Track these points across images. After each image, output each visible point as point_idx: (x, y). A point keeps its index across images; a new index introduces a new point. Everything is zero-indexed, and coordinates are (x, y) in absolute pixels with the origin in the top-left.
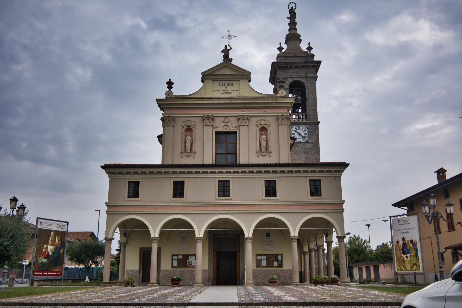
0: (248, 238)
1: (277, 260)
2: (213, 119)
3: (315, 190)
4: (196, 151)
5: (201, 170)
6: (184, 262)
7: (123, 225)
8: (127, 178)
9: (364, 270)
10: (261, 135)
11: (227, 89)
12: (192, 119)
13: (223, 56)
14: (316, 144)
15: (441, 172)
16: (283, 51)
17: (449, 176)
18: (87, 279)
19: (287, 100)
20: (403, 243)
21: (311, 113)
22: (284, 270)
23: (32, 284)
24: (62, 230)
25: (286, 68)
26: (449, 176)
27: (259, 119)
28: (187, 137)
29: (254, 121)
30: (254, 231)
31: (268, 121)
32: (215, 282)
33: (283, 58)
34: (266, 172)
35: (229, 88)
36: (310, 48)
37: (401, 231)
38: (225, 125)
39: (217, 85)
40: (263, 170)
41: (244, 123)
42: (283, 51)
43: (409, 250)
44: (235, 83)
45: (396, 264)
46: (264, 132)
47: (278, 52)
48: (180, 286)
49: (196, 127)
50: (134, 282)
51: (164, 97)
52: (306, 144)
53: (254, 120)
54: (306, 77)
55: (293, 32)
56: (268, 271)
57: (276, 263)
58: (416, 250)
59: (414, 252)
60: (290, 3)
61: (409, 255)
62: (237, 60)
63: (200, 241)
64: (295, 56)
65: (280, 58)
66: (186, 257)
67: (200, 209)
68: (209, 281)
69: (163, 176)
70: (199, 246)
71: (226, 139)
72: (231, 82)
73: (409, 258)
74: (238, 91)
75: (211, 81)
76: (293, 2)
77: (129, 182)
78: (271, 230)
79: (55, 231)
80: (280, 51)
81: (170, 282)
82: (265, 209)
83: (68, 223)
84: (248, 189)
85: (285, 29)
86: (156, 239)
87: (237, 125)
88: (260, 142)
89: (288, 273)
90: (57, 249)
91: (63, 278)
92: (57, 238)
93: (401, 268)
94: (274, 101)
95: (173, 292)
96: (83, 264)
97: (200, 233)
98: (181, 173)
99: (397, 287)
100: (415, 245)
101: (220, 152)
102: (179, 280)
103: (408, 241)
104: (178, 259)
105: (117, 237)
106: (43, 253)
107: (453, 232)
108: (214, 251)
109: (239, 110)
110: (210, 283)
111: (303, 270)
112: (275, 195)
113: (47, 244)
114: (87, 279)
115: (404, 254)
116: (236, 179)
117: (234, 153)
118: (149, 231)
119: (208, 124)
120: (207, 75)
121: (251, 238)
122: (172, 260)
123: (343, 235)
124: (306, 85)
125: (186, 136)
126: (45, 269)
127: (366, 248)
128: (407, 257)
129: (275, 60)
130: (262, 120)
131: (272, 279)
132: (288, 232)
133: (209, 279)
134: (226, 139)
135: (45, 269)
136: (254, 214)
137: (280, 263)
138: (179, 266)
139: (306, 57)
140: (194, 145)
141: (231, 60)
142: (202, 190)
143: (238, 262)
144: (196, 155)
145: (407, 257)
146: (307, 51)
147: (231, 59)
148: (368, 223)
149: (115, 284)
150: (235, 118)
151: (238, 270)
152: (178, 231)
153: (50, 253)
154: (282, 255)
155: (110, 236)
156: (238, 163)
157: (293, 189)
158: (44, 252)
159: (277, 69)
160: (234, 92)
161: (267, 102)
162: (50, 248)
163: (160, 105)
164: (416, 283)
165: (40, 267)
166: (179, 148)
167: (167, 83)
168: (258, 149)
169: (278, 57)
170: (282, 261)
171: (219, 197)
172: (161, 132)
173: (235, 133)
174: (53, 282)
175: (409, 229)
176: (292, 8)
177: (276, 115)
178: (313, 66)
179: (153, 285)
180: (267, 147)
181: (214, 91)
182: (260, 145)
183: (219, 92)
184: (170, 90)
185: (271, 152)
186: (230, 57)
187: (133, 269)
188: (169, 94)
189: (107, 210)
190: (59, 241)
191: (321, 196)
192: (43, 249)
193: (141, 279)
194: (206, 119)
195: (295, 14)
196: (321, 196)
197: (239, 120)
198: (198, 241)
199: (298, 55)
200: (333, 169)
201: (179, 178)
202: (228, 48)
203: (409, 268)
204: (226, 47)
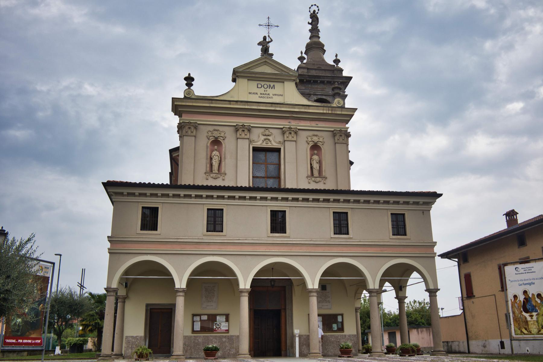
1: (336, 322)
2: (249, 130)
3: (399, 226)
4: (227, 172)
10: (312, 155)
11: (267, 93)
15: (511, 215)
16: (305, 61)
17: (521, 219)
18: (58, 351)
22: (345, 336)
26: (521, 219)
28: (214, 153)
31: (321, 137)
33: (306, 71)
35: (270, 91)
36: (337, 61)
37: (522, 282)
38: (265, 139)
39: (253, 86)
40: (332, 197)
44: (277, 85)
45: (513, 326)
46: (316, 152)
49: (226, 140)
55: (315, 40)
57: (335, 326)
60: (312, 5)
61: (534, 314)
64: (319, 69)
65: (302, 70)
67: (246, 248)
69: (193, 201)
72: (272, 84)
73: (535, 318)
74: (282, 95)
76: (315, 5)
78: (342, 281)
80: (302, 62)
81: (203, 354)
85: (305, 38)
88: (311, 164)
91: (44, 348)
93: (522, 331)
94: (330, 112)
101: (258, 174)
102: (216, 350)
103: (533, 295)
104: (201, 320)
114: (58, 351)
115: (527, 311)
116: (294, 208)
117: (278, 177)
119: (243, 136)
120: (241, 72)
122: (193, 322)
125: (212, 151)
126: (19, 334)
128: (531, 316)
131: (346, 348)
135: (19, 334)
137: (340, 326)
139: (333, 71)
140: (223, 163)
141: (272, 55)
142: (248, 221)
143: (283, 325)
145: (531, 316)
147: (272, 55)
150: (279, 131)
152: (212, 280)
154: (342, 315)
160: (276, 96)
161: (322, 111)
164: (469, 352)
167: (186, 79)
170: (342, 323)
173: (278, 150)
174: (6, 354)
175: (533, 279)
176: (314, 11)
177: (333, 129)
180: (320, 171)
181: (250, 93)
182: (312, 168)
183: (257, 96)
184: (189, 88)
185: (326, 178)
186: (270, 52)
187: (135, 335)
188: (189, 94)
195: (318, 19)
197: (284, 133)
200: (421, 200)
201: (215, 204)
202: (267, 40)
204: (265, 38)
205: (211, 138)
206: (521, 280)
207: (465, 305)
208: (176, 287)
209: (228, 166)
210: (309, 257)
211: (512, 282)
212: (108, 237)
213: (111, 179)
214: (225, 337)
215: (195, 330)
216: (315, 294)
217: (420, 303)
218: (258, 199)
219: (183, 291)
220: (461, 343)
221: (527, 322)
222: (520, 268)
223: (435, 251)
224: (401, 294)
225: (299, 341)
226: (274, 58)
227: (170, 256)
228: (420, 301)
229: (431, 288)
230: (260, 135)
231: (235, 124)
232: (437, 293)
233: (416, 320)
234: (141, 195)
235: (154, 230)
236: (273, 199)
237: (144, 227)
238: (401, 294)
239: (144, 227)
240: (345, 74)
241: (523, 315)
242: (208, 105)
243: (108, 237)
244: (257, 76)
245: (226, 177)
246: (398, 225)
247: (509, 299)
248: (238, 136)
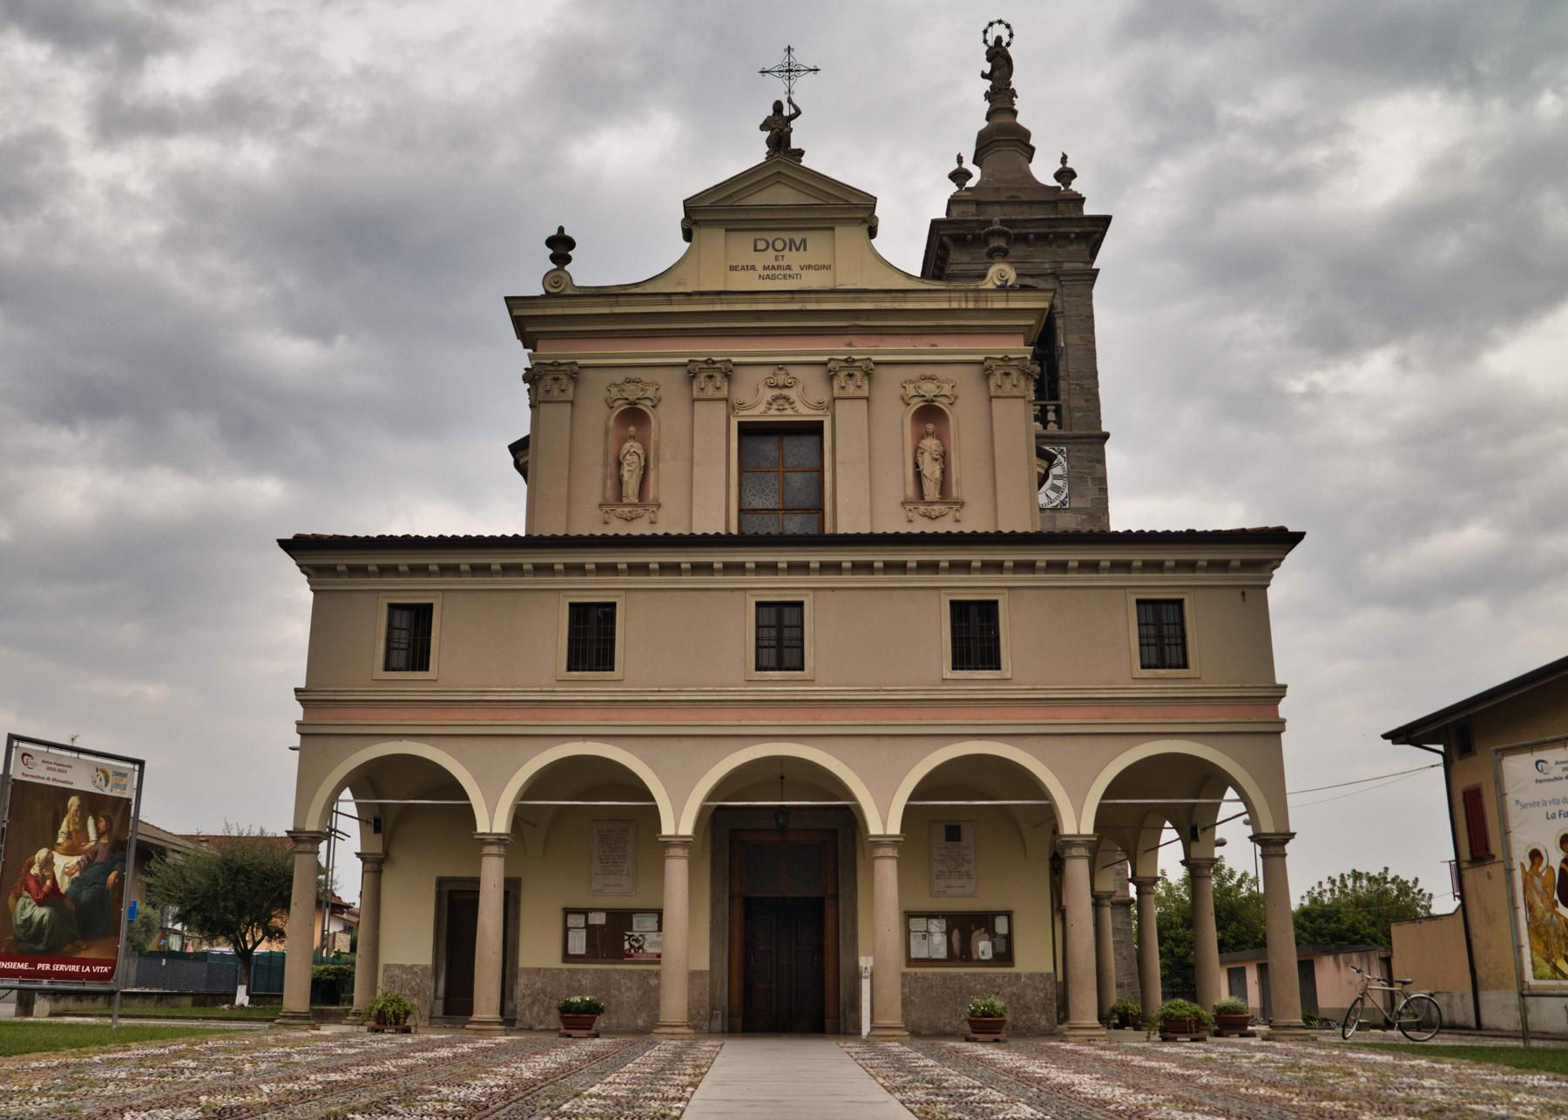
0: (879, 842)
2: (728, 376)
3: (1163, 636)
5: (685, 558)
6: (612, 937)
7: (365, 781)
8: (383, 593)
9: (1252, 977)
10: (920, 437)
11: (785, 263)
13: (769, 142)
16: (971, 183)
18: (242, 997)
21: (1076, 402)
22: (1018, 976)
23: (25, 1006)
24: (116, 793)
28: (627, 446)
30: (909, 811)
31: (947, 381)
32: (738, 1021)
33: (972, 209)
34: (955, 567)
35: (794, 258)
36: (1066, 175)
37: (1553, 809)
38: (776, 399)
39: (742, 247)
40: (944, 556)
41: (851, 390)
42: (971, 183)
44: (815, 240)
45: (1526, 951)
46: (930, 427)
47: (953, 188)
48: (597, 1036)
49: (662, 407)
50: (407, 1013)
52: (1058, 515)
53: (891, 381)
54: (1055, 275)
55: (1003, 119)
56: (952, 977)
57: (984, 948)
60: (991, 24)
62: (824, 152)
63: (679, 851)
64: (1013, 202)
66: (620, 920)
67: (682, 719)
68: (712, 1017)
70: (677, 871)
71: (779, 447)
72: (798, 237)
74: (829, 267)
75: (723, 231)
76: (1000, 22)
77: (392, 607)
78: (974, 811)
79: (84, 795)
80: (960, 185)
81: (554, 1020)
83: (141, 763)
84: (879, 637)
85: (976, 116)
86: (499, 840)
87: (824, 397)
88: (916, 465)
89: (1036, 988)
90: (92, 870)
92: (91, 822)
93: (1555, 968)
94: (971, 305)
95: (567, 1070)
96: (228, 938)
97: (679, 818)
98: (601, 569)
99: (1537, 1050)
101: (757, 503)
102: (593, 1010)
104: (588, 927)
105: (349, 825)
106: (32, 884)
108: (732, 896)
110: (717, 1025)
112: (997, 666)
113: (52, 845)
114: (242, 997)
116: (829, 593)
118: (469, 809)
120: (705, 210)
121: (893, 842)
122: (566, 930)
123: (1283, 830)
126: (41, 947)
129: (941, 214)
131: (984, 1014)
132: (1049, 815)
133: (713, 1008)
134: (779, 447)
135: (41, 947)
136: (912, 741)
137: (1002, 949)
138: (592, 954)
142: (687, 638)
146: (1054, 183)
147: (800, 153)
149: (337, 1018)
150: (819, 371)
151: (829, 977)
152: (589, 811)
153: (64, 885)
154: (1009, 914)
155: (312, 825)
157: (1065, 639)
158: (35, 877)
160: (811, 272)
161: (945, 305)
162: (64, 865)
163: (520, 324)
164: (1479, 1026)
165: (18, 941)
166: (593, 485)
167: (551, 242)
168: (911, 490)
169: (952, 202)
170: (1009, 938)
171: (758, 669)
172: (524, 430)
173: (815, 429)
176: (999, 39)
177: (981, 358)
179: (484, 1028)
182: (918, 476)
183: (754, 275)
185: (962, 504)
186: (794, 145)
187: (408, 963)
188: (557, 284)
190: (99, 835)
191: (1185, 666)
192: (31, 865)
193: (440, 1003)
196: (1185, 666)
197: (831, 376)
198: (672, 851)
199: (1024, 198)
200: (1235, 555)
201: (593, 590)
202: (786, 113)
204: (778, 107)
205: (617, 404)
206: (1555, 802)
207: (1468, 884)
208: (480, 830)
210: (872, 741)
211: (1524, 806)
212: (297, 690)
215: (571, 952)
216: (1083, 851)
217: (1370, 879)
218: (719, 571)
220: (1457, 1000)
222: (1551, 763)
223: (1281, 715)
224: (1198, 852)
226: (806, 162)
227: (462, 742)
228: (1374, 873)
229: (1264, 830)
230: (761, 388)
231: (686, 360)
232: (1289, 847)
233: (1353, 929)
234: (384, 570)
235: (421, 669)
236: (761, 568)
238: (1198, 852)
240: (1089, 210)
241: (1558, 915)
242: (606, 310)
243: (297, 690)
244: (751, 216)
245: (661, 514)
246: (1160, 637)
247: (1516, 865)
248: (696, 394)
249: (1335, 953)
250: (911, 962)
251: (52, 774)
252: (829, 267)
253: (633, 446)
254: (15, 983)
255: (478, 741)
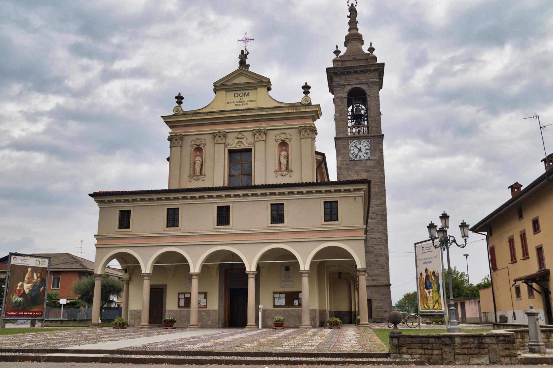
2: (225, 136)
4: (206, 174)
8: (119, 206)
11: (243, 100)
12: (201, 137)
14: (380, 162)
19: (311, 108)
20: (426, 276)
21: (374, 125)
24: (43, 266)
25: (343, 73)
27: (279, 132)
29: (272, 135)
32: (227, 324)
33: (340, 63)
35: (245, 99)
36: (371, 50)
37: (424, 261)
38: (238, 142)
39: (230, 96)
41: (260, 138)
43: (431, 284)
46: (284, 148)
47: (334, 56)
49: (206, 147)
51: (171, 113)
52: (367, 162)
53: (272, 134)
54: (367, 83)
55: (353, 31)
56: (286, 311)
57: (296, 302)
58: (438, 284)
59: (436, 286)
61: (431, 290)
63: (195, 277)
64: (355, 60)
65: (337, 63)
68: (219, 323)
70: (305, 280)
71: (240, 158)
72: (247, 92)
73: (431, 293)
74: (255, 101)
79: (33, 268)
80: (337, 55)
82: (271, 238)
92: (35, 274)
94: (295, 111)
97: (305, 265)
100: (437, 277)
101: (234, 173)
104: (185, 298)
106: (17, 292)
107: (527, 260)
108: (226, 288)
109: (255, 123)
110: (220, 325)
111: (357, 310)
113: (23, 281)
115: (427, 289)
119: (220, 141)
120: (219, 86)
122: (179, 299)
124: (368, 92)
126: (20, 308)
127: (462, 281)
128: (429, 292)
130: (282, 133)
131: (276, 321)
133: (219, 320)
134: (240, 158)
135: (20, 308)
140: (203, 166)
142: (199, 218)
144: (206, 178)
145: (429, 292)
146: (368, 52)
147: (249, 66)
148: (466, 253)
150: (251, 133)
152: (280, 263)
153: (27, 291)
156: (253, 184)
158: (18, 290)
159: (333, 76)
161: (287, 111)
165: (13, 307)
166: (187, 170)
167: (176, 98)
168: (277, 168)
171: (325, 221)
172: (169, 156)
173: (250, 150)
174: (64, 322)
175: (431, 258)
176: (352, 5)
177: (298, 126)
178: (375, 70)
180: (287, 165)
181: (228, 103)
182: (280, 163)
183: (234, 104)
185: (292, 171)
186: (247, 64)
187: (136, 309)
188: (177, 110)
189: (96, 243)
190: (38, 278)
192: (17, 286)
194: (217, 136)
195: (356, 11)
198: (304, 275)
199: (358, 58)
203: (431, 306)
209: (207, 169)
210: (247, 245)
213: (98, 191)
214: (204, 311)
219: (307, 272)
221: (427, 298)
225: (262, 316)
226: (250, 69)
234: (118, 201)
237: (121, 226)
239: (121, 226)
242: (190, 118)
248: (215, 142)
249: (469, 300)
250: (275, 306)
251: (23, 262)
252: (255, 101)
253: (199, 158)
254: (30, 318)
255: (142, 248)
